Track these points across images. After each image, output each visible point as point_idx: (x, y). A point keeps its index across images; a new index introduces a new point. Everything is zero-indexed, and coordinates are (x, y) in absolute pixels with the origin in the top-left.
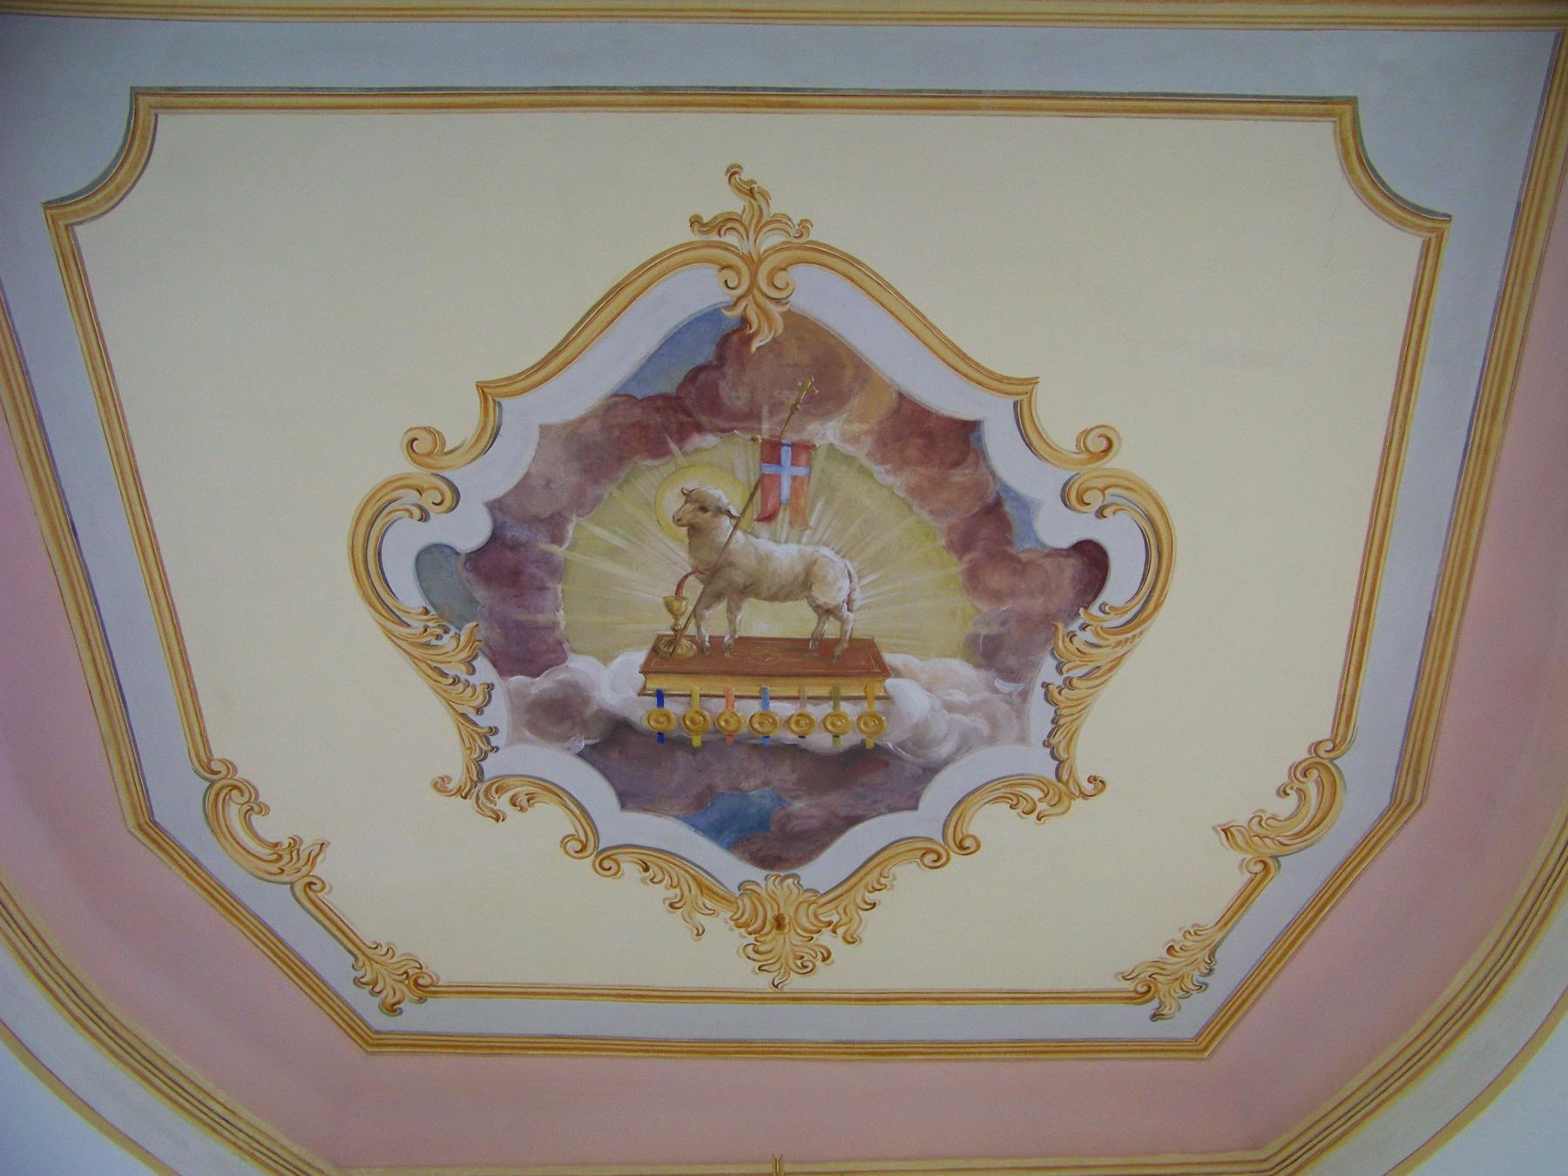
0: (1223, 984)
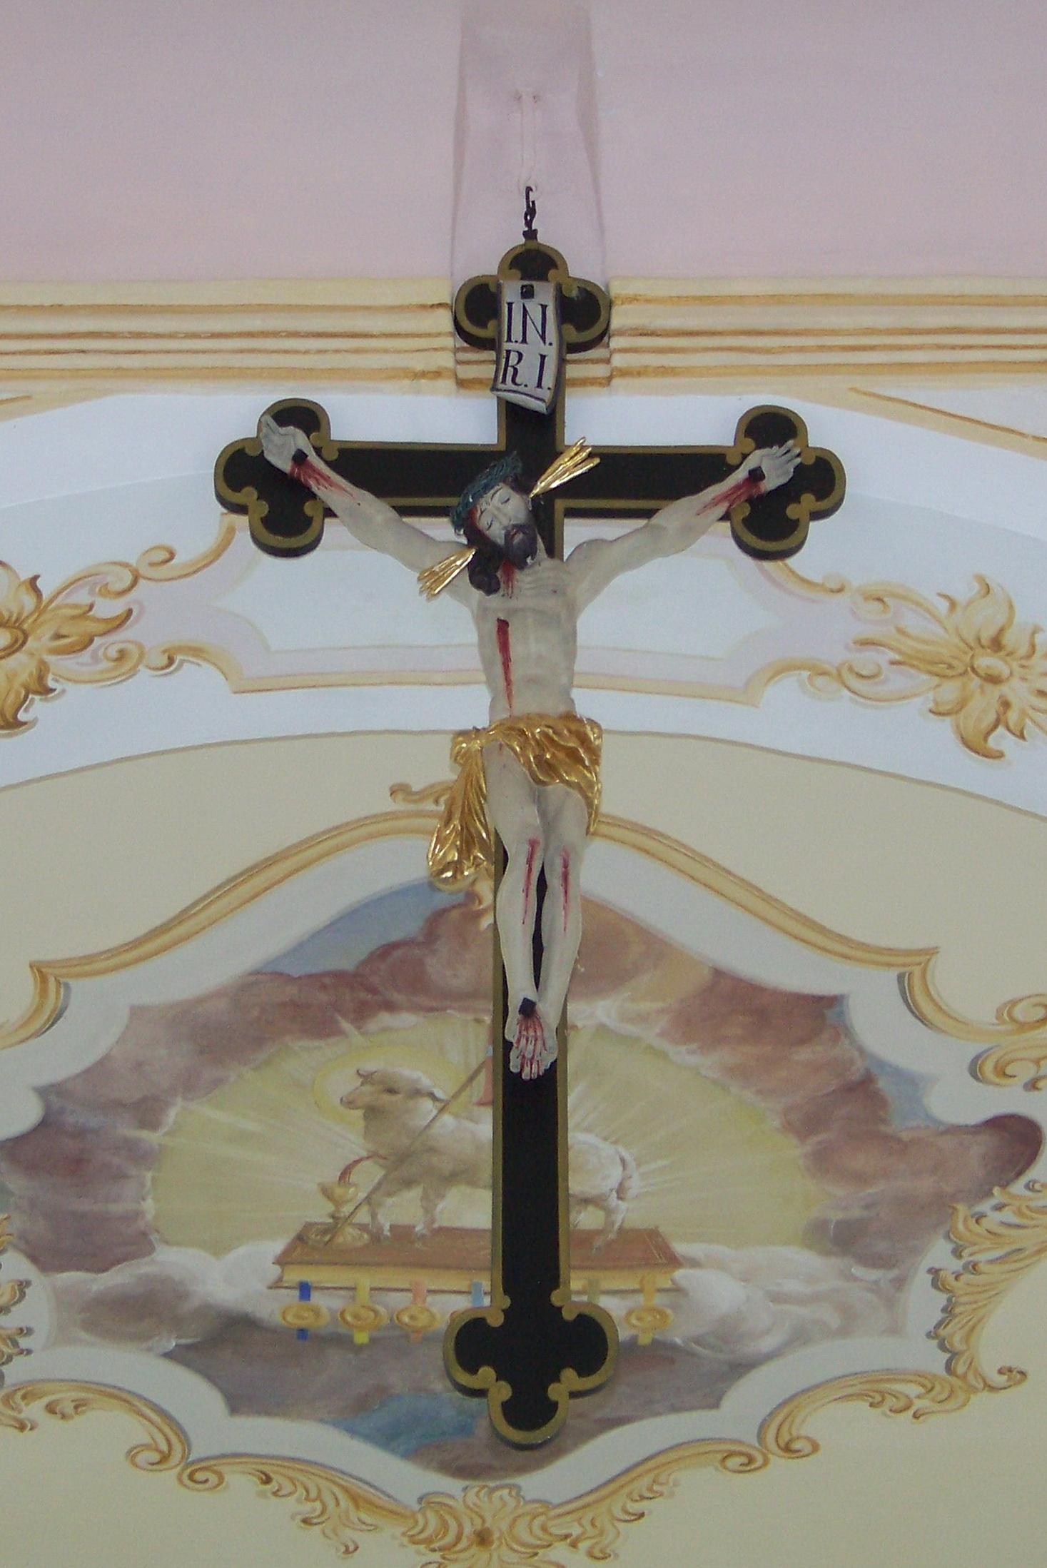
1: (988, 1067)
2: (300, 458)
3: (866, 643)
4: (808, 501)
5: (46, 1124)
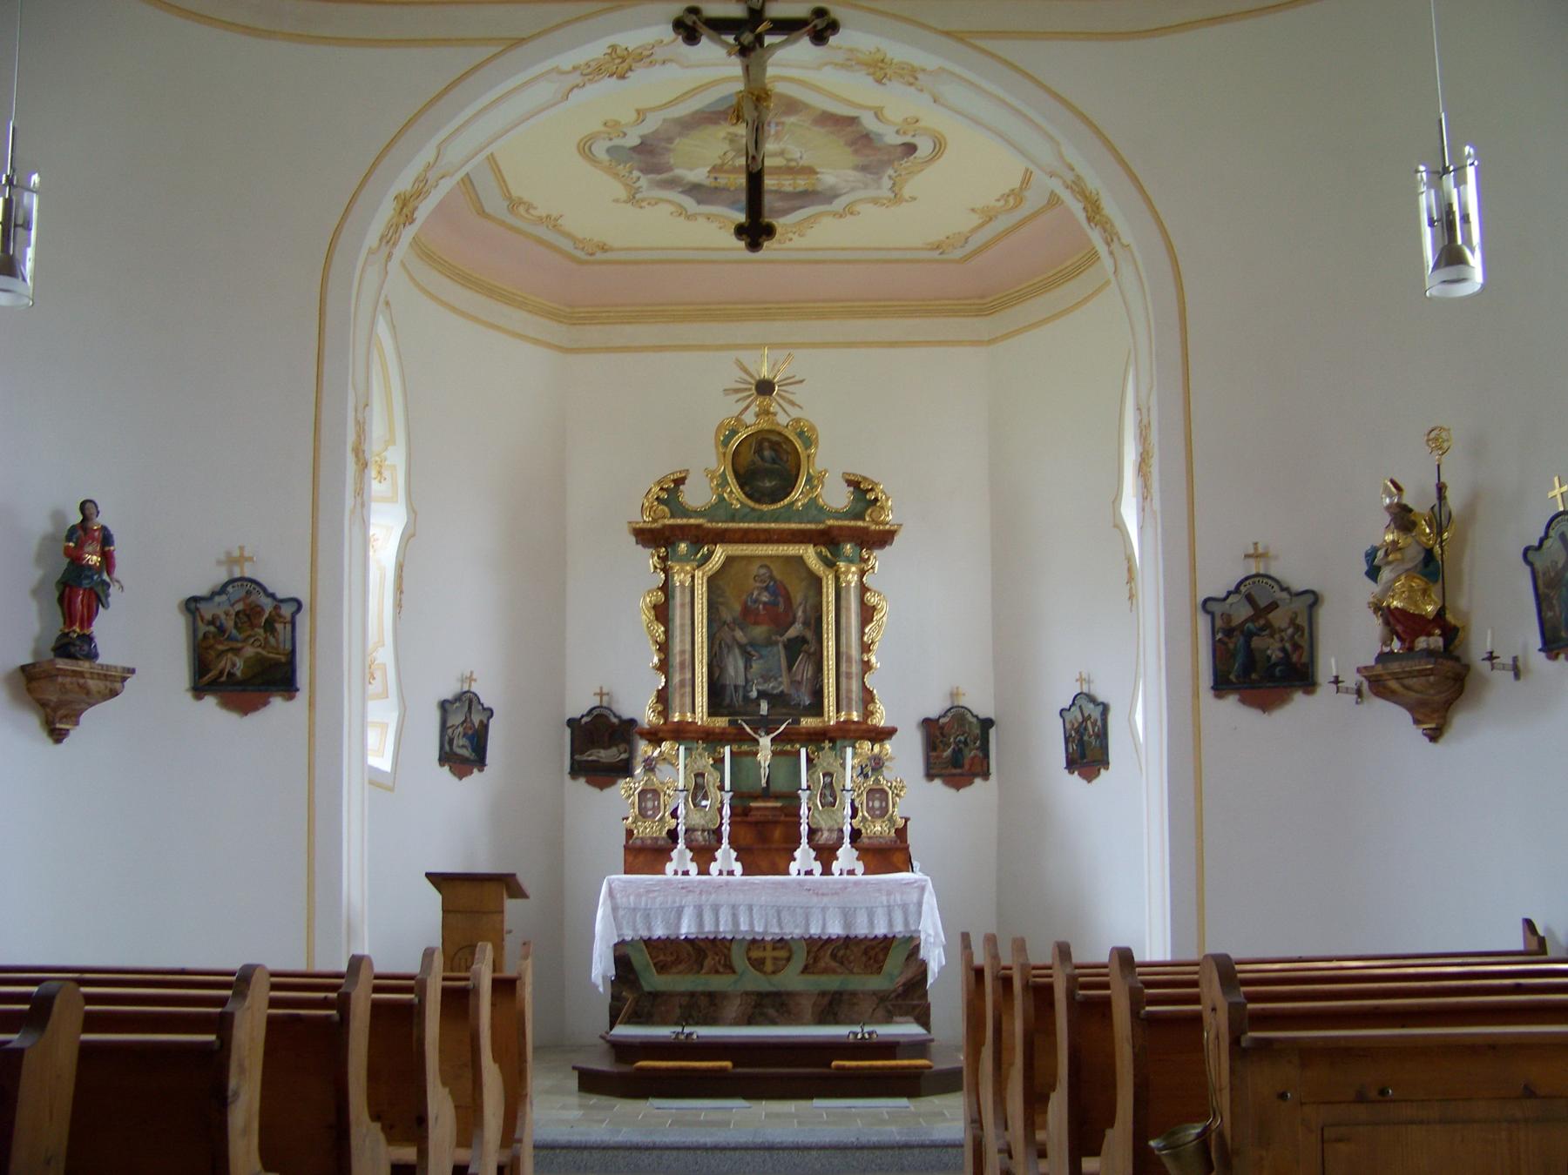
0: (970, 247)
1: (901, 132)
2: (694, 23)
3: (848, 60)
4: (829, 32)
5: (642, 143)
